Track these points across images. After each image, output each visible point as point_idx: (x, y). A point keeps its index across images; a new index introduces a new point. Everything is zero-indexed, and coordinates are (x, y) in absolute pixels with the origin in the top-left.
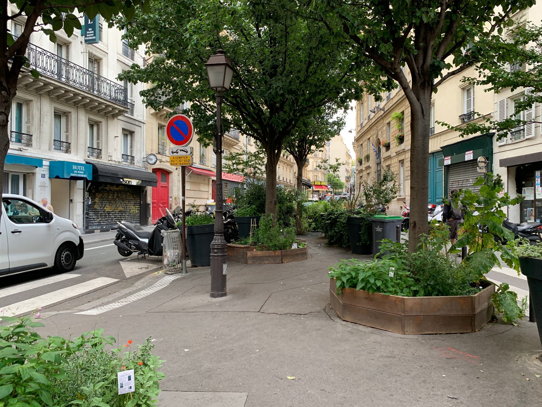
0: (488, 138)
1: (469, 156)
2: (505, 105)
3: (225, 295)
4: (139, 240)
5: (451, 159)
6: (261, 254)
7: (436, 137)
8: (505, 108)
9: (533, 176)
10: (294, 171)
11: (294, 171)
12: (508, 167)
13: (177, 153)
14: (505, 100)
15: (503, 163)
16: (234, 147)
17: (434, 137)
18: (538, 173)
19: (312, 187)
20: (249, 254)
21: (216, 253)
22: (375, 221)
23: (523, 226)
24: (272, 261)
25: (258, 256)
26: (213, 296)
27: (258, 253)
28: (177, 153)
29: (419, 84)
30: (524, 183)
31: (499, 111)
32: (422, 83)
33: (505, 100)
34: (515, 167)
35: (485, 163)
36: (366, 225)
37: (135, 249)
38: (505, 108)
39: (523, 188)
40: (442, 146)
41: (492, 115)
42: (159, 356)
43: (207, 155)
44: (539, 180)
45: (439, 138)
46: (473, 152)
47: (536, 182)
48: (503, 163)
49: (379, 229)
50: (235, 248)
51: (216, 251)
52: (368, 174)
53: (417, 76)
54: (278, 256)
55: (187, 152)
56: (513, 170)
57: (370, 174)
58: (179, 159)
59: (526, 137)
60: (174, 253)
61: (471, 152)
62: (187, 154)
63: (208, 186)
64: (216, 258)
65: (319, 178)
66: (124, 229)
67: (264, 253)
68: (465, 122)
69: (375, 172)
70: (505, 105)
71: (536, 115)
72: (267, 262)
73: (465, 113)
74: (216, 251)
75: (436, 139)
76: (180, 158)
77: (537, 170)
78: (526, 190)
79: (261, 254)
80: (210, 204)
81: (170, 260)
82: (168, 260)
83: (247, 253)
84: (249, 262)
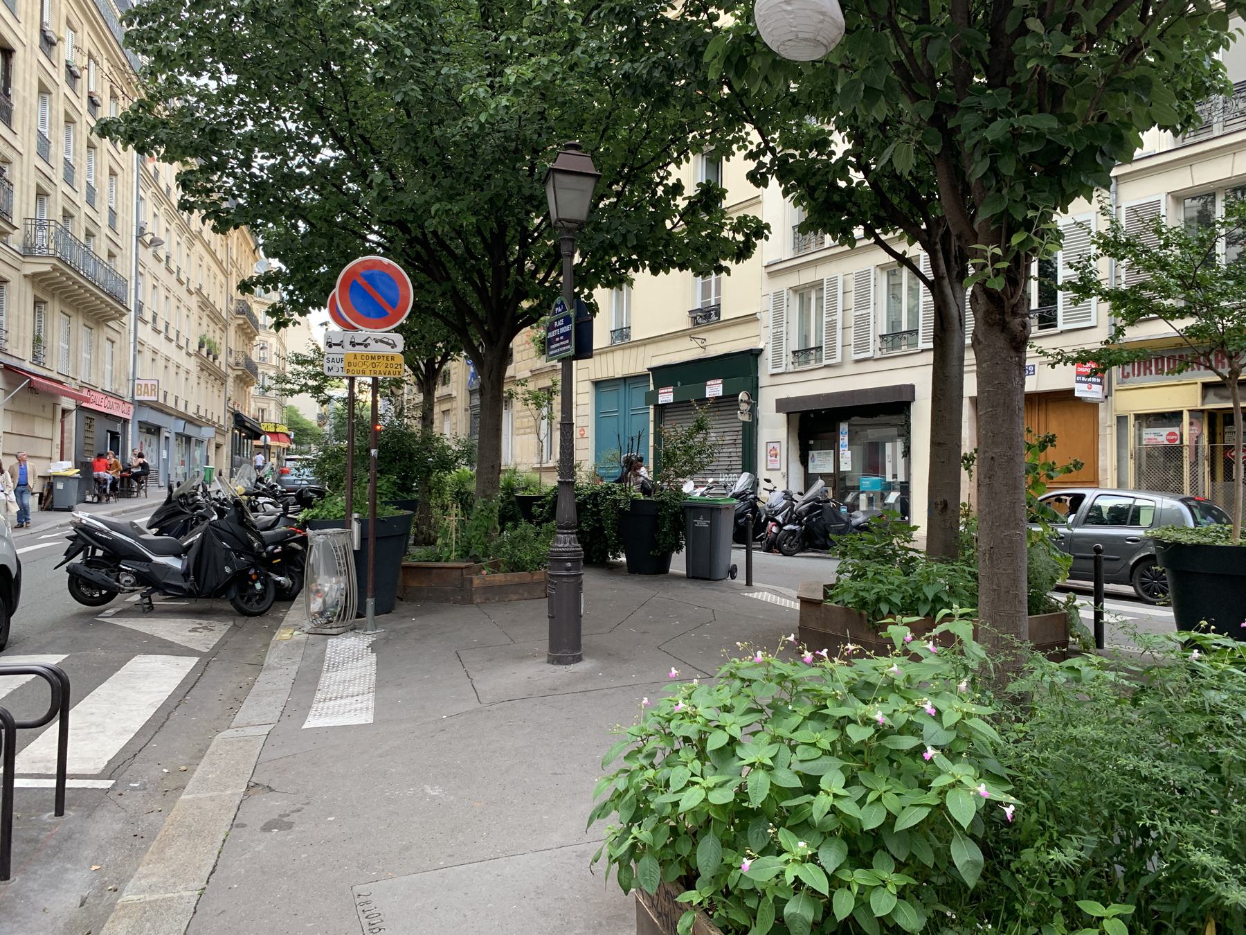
0: (751, 358)
1: (714, 389)
2: (785, 300)
3: (578, 659)
4: (151, 560)
5: (673, 392)
6: (503, 579)
7: (634, 347)
8: (785, 306)
9: (836, 431)
10: (228, 395)
11: (228, 395)
12: (788, 414)
13: (366, 346)
14: (785, 292)
15: (781, 405)
16: (110, 323)
17: (630, 348)
18: (844, 427)
19: (263, 437)
20: (477, 581)
21: (568, 569)
22: (694, 507)
23: (856, 517)
24: (526, 595)
25: (498, 584)
26: (555, 660)
27: (497, 578)
28: (366, 346)
29: (955, 273)
30: (812, 442)
31: (771, 311)
32: (958, 272)
33: (785, 292)
34: (798, 415)
35: (748, 403)
36: (672, 515)
37: (132, 585)
38: (785, 306)
39: (811, 453)
40: (649, 366)
41: (758, 315)
42: (96, 864)
43: (49, 339)
44: (846, 438)
45: (641, 349)
46: (723, 383)
47: (841, 442)
48: (781, 405)
49: (702, 523)
50: (435, 571)
51: (569, 564)
52: (443, 412)
53: (953, 259)
54: (539, 583)
55: (394, 346)
56: (796, 418)
57: (452, 413)
58: (370, 361)
59: (825, 362)
60: (338, 582)
61: (720, 381)
62: (395, 350)
63: (50, 424)
64: (565, 580)
65: (270, 415)
66: (101, 531)
67: (509, 578)
68: (698, 324)
69: (466, 410)
70: (785, 300)
71: (843, 324)
72: (515, 597)
73: (699, 307)
74: (569, 564)
75: (634, 351)
76: (373, 358)
77: (842, 421)
78: (816, 455)
79: (503, 579)
80: (62, 473)
81: (329, 601)
82: (324, 602)
83: (471, 579)
84: (477, 599)
